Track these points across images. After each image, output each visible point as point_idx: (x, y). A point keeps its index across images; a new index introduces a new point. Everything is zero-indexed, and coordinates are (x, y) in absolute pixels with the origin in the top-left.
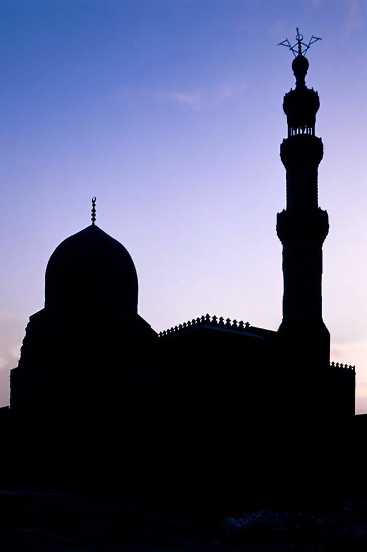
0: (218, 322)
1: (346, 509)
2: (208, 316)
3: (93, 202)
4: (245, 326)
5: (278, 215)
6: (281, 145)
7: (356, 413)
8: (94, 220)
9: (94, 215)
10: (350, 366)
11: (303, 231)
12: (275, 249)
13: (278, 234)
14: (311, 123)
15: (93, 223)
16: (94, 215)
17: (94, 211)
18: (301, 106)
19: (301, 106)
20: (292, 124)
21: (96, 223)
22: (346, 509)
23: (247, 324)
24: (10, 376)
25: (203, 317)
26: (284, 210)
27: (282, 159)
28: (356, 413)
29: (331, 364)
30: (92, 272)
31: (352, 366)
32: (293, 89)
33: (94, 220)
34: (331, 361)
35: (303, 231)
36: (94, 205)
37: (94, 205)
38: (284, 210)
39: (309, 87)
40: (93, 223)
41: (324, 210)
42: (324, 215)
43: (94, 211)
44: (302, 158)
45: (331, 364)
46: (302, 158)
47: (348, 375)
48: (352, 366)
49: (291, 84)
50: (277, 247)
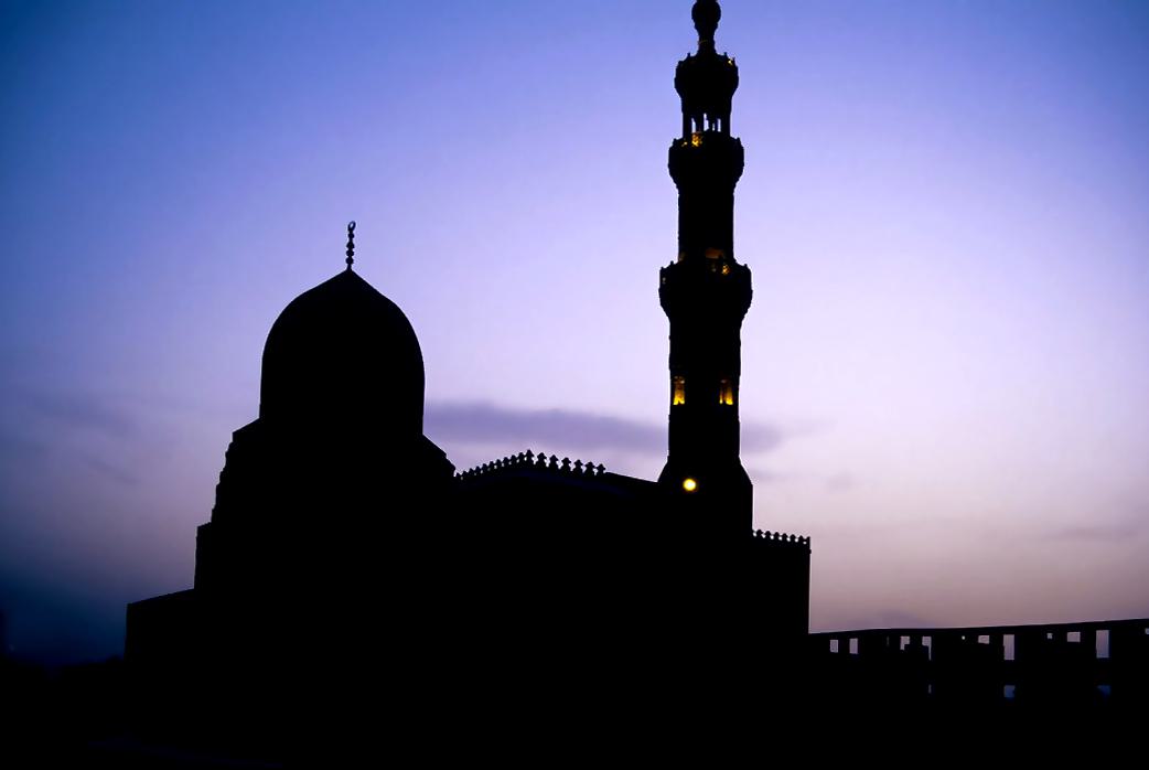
0: (547, 465)
1: (930, 691)
2: (530, 454)
3: (351, 230)
4: (596, 471)
5: (663, 272)
6: (671, 149)
7: (810, 632)
8: (350, 261)
9: (350, 253)
10: (801, 538)
11: (706, 302)
12: (657, 328)
13: (661, 291)
14: (722, 111)
15: (349, 267)
16: (350, 253)
17: (351, 245)
18: (707, 83)
19: (707, 83)
20: (690, 111)
21: (353, 268)
22: (930, 691)
23: (601, 468)
24: (213, 511)
25: (521, 455)
26: (672, 262)
27: (672, 174)
28: (810, 632)
29: (755, 535)
30: (343, 352)
31: (805, 537)
32: (693, 54)
33: (350, 261)
34: (755, 528)
35: (706, 302)
36: (351, 236)
37: (351, 236)
38: (672, 262)
39: (720, 52)
40: (349, 267)
41: (743, 264)
42: (743, 274)
43: (351, 245)
44: (707, 174)
45: (755, 535)
46: (707, 174)
47: (793, 554)
48: (805, 537)
49: (690, 45)
50: (662, 324)
